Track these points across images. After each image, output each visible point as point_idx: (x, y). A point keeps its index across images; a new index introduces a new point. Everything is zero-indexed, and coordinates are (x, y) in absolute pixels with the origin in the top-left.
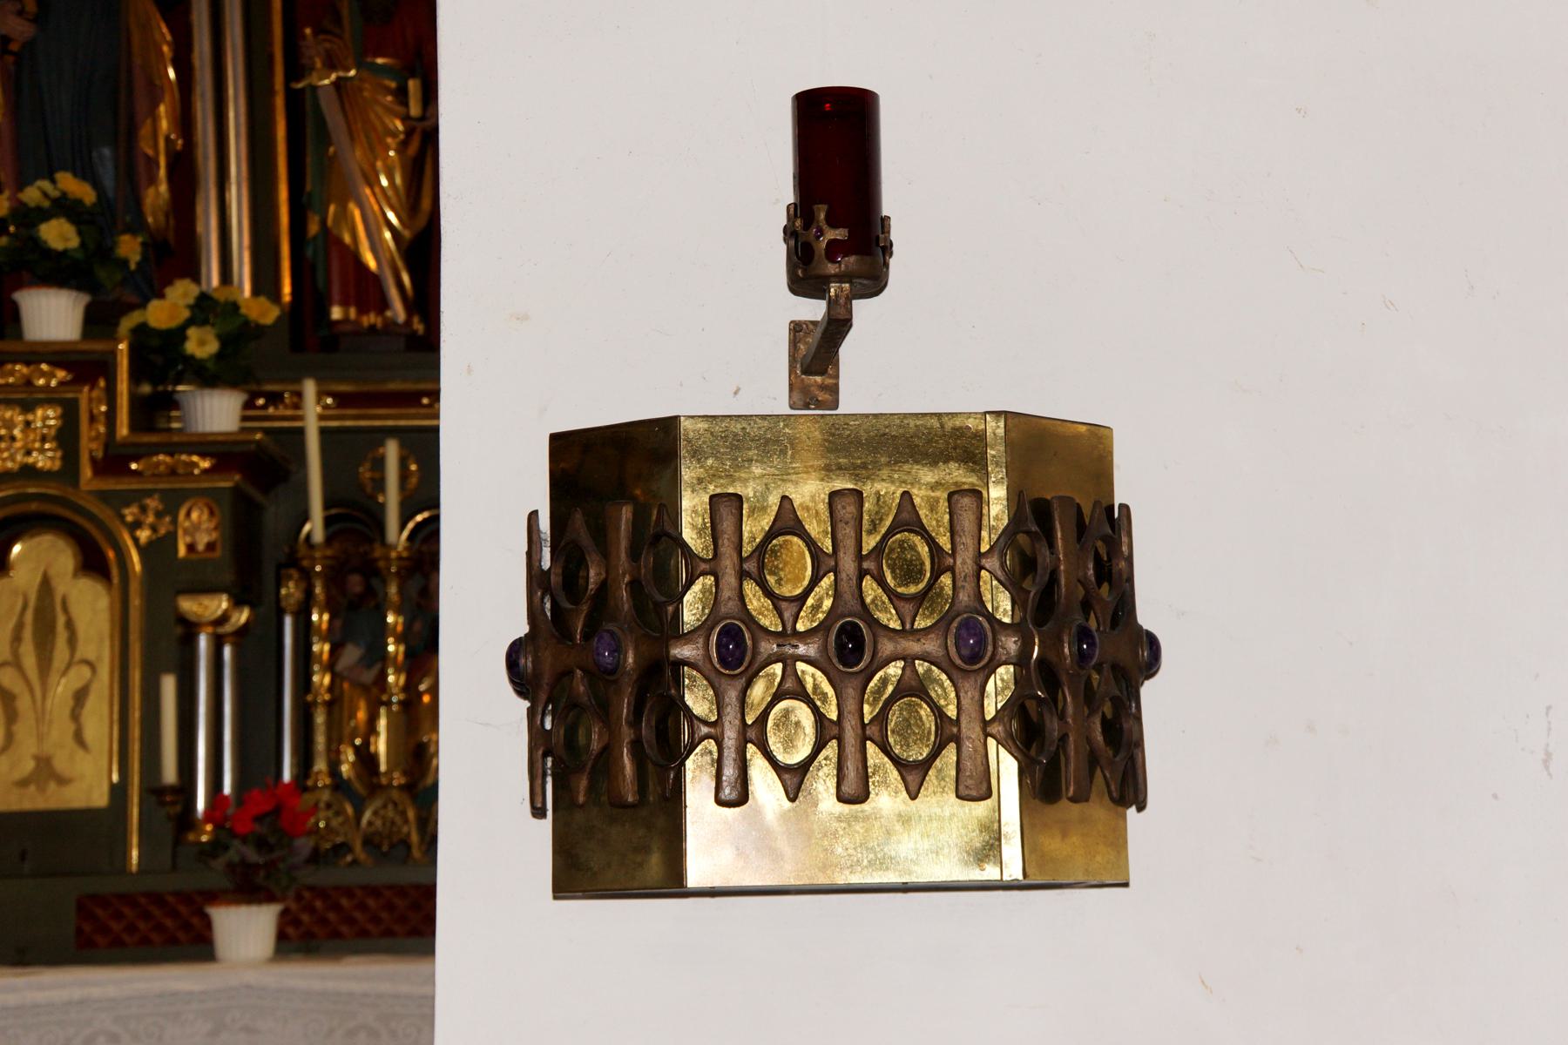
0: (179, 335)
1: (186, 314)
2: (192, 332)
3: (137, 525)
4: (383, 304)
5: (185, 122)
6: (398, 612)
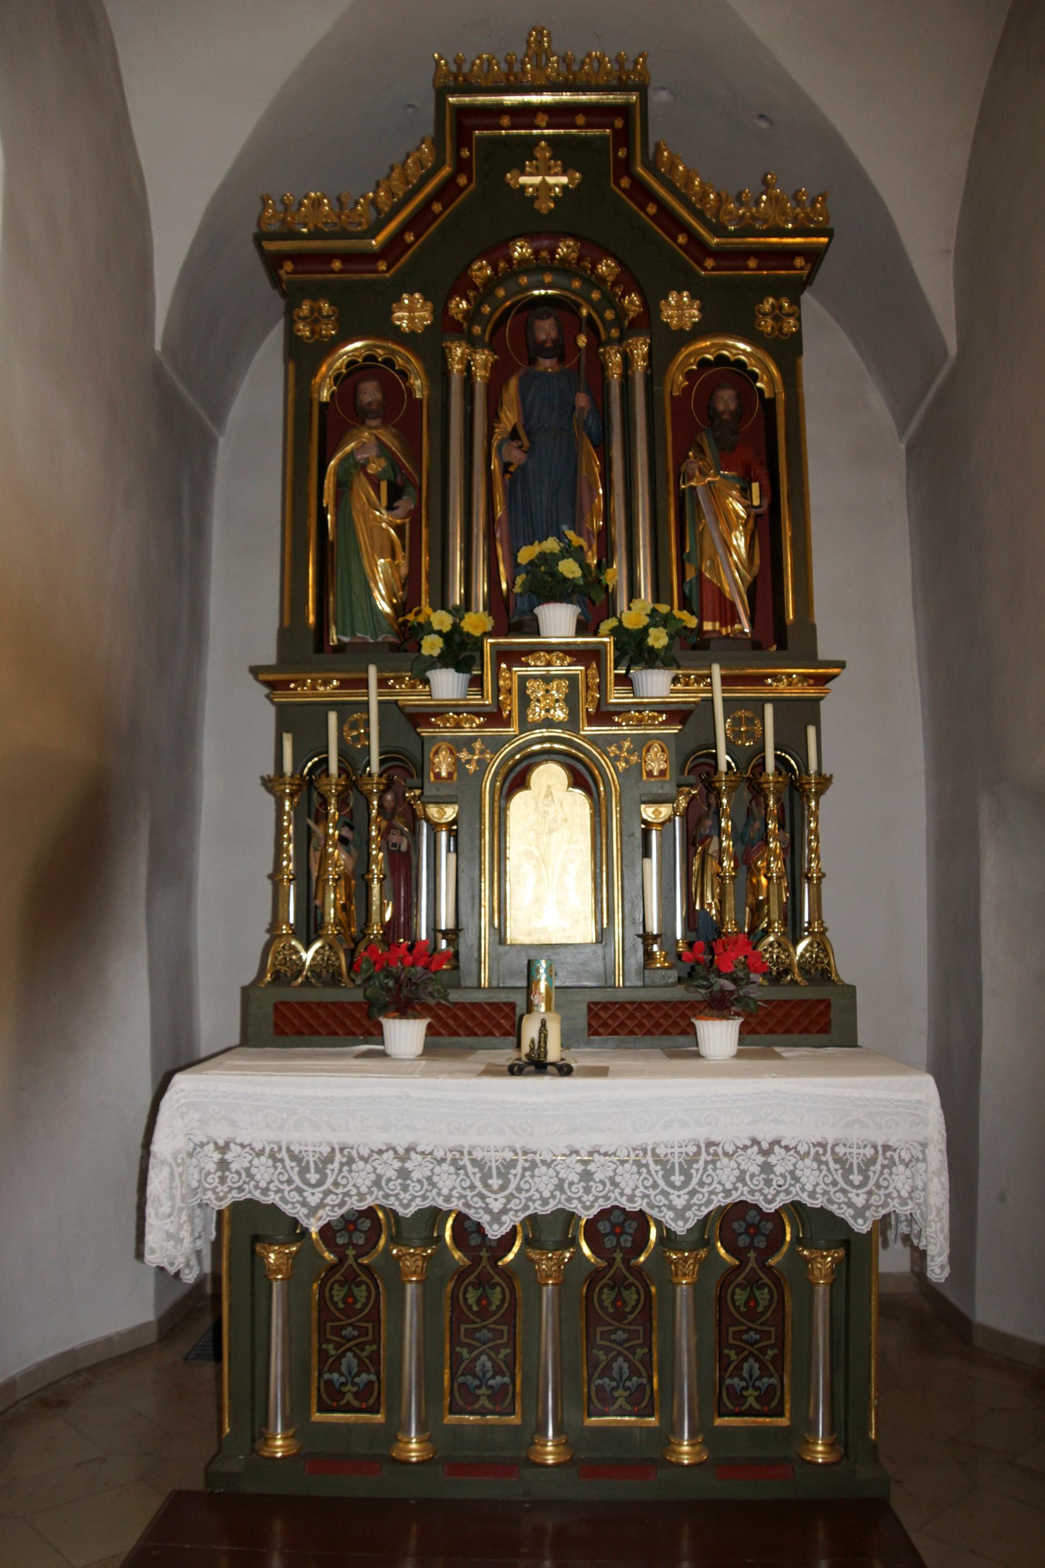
0: (644, 632)
1: (647, 620)
2: (652, 631)
3: (617, 758)
4: (735, 618)
5: (607, 516)
6: (729, 818)
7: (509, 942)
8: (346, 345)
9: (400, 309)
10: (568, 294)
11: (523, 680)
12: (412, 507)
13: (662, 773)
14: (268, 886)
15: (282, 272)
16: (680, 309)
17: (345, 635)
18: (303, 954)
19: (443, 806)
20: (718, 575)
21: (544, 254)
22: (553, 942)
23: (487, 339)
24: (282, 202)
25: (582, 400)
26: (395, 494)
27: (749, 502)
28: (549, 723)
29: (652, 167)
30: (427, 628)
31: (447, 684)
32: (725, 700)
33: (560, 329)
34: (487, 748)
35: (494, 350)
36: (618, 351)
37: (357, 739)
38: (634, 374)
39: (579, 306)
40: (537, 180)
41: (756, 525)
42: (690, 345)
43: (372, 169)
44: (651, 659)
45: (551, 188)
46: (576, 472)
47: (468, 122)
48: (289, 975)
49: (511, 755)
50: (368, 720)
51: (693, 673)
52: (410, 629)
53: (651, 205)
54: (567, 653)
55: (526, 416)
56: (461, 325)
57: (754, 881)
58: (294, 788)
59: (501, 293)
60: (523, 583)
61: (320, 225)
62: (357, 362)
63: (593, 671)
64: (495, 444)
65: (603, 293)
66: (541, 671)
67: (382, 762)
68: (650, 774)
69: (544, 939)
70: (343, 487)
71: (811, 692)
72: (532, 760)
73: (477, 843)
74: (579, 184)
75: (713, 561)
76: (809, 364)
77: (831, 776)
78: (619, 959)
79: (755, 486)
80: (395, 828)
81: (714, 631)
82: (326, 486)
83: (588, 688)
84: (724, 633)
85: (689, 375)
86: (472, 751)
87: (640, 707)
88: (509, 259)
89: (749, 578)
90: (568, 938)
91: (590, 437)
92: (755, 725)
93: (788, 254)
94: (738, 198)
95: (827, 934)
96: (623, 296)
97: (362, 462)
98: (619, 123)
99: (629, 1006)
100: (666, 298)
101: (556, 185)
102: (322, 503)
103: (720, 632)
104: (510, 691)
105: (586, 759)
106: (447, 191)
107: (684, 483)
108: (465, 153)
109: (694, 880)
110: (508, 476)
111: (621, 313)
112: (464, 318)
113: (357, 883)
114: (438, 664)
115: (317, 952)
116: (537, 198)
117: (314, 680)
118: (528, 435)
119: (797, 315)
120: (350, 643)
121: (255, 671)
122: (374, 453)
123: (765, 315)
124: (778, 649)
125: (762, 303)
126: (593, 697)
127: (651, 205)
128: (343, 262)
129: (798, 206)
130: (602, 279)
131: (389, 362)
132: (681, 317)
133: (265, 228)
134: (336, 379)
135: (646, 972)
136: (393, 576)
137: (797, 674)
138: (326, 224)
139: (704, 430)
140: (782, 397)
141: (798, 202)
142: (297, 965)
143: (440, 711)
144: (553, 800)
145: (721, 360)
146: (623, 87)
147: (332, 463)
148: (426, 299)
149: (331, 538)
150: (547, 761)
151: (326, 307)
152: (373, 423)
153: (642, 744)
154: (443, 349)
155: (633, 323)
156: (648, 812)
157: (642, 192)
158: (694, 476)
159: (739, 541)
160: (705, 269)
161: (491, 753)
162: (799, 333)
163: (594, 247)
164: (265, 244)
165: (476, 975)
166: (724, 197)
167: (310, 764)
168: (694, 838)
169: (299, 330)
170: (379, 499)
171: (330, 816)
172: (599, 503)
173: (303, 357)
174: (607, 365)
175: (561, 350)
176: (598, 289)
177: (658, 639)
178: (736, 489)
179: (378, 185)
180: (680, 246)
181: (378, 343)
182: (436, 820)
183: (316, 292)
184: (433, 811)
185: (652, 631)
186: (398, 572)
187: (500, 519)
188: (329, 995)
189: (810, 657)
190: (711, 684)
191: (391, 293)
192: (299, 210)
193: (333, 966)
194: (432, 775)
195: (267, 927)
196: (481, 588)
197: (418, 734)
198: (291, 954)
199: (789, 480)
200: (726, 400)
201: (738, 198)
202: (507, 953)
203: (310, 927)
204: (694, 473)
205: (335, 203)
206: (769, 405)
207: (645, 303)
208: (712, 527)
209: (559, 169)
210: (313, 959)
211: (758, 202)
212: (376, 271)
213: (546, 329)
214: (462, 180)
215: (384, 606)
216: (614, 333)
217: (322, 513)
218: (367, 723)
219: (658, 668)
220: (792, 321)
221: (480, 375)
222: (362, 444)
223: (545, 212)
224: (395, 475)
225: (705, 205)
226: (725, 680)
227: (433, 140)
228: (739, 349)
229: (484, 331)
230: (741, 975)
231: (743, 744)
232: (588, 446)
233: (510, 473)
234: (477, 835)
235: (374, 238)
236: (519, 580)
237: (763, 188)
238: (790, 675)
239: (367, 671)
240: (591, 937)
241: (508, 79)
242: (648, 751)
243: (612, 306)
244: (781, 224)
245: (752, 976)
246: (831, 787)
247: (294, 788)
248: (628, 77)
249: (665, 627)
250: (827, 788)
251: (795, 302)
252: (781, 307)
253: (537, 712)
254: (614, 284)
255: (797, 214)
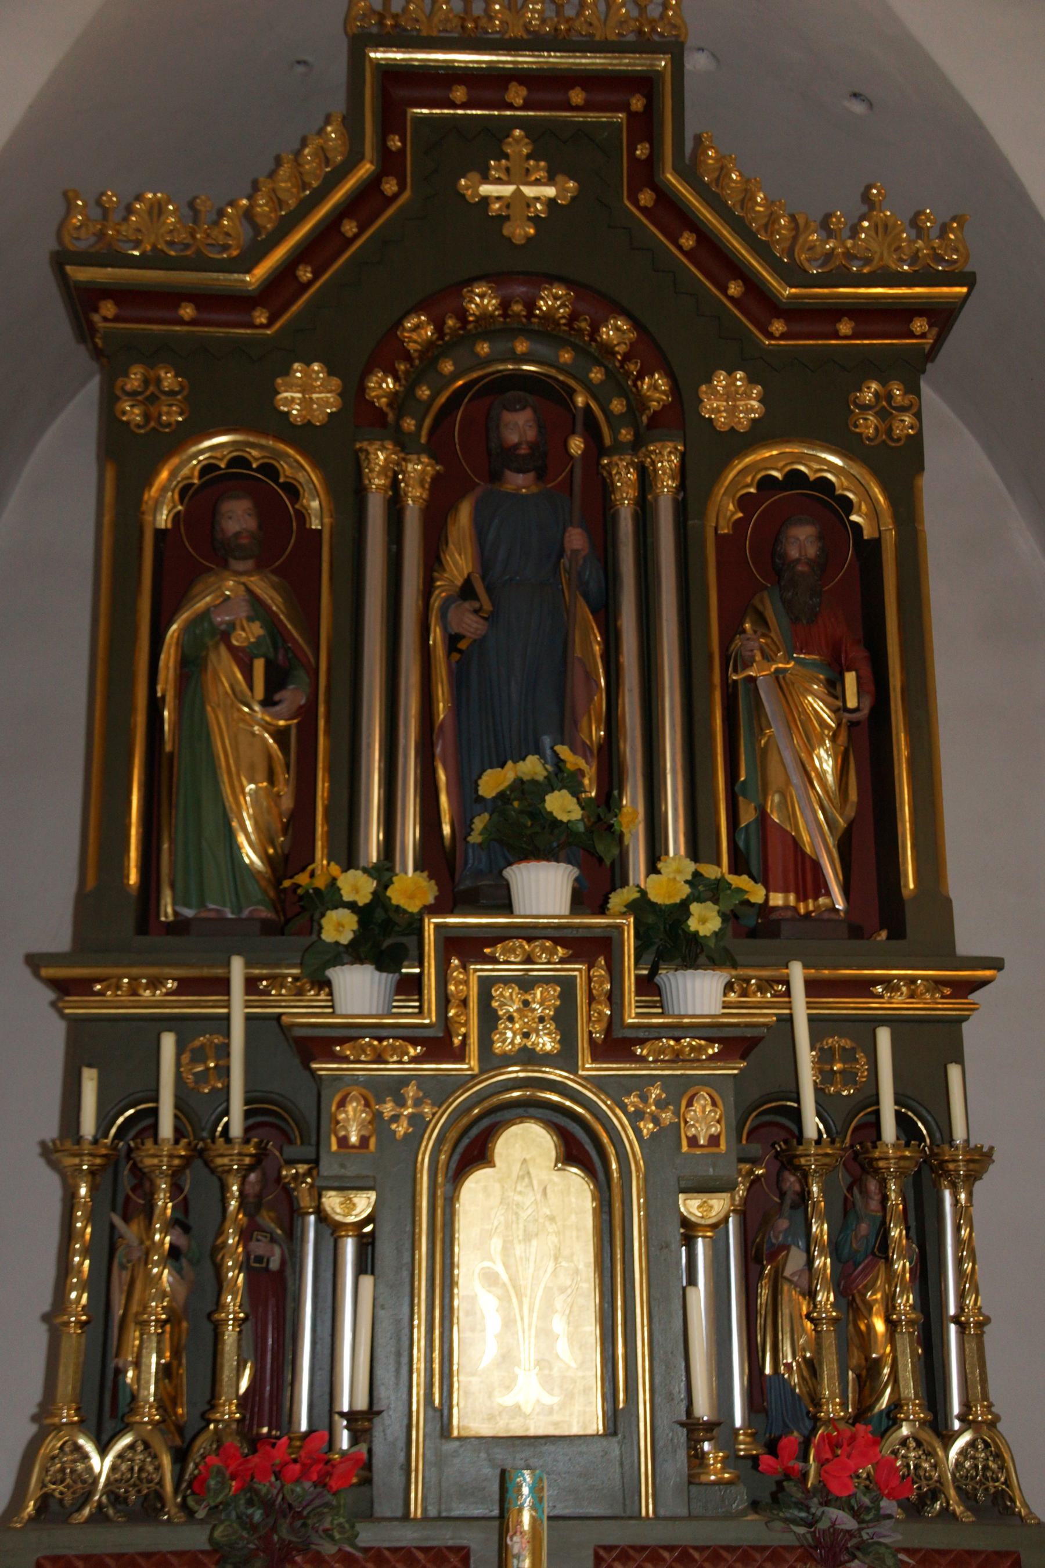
0: (683, 908)
1: (687, 890)
4: (820, 887)
5: (612, 722)
7: (455, 1433)
8: (201, 441)
9: (289, 388)
10: (553, 372)
11: (486, 985)
12: (303, 702)
13: (714, 1140)
14: (41, 1333)
15: (96, 318)
16: (731, 399)
17: (187, 905)
18: (95, 1460)
19: (352, 1194)
20: (792, 818)
21: (517, 308)
22: (532, 1432)
23: (423, 440)
24: (99, 203)
25: (576, 539)
26: (276, 681)
27: (840, 704)
28: (528, 1056)
29: (690, 173)
30: (329, 897)
31: (358, 991)
32: (811, 1019)
33: (541, 426)
34: (426, 1095)
35: (435, 457)
36: (631, 463)
37: (202, 1077)
38: (656, 498)
39: (571, 392)
40: (507, 190)
41: (850, 738)
42: (746, 455)
43: (252, 175)
44: (691, 953)
45: (529, 203)
46: (565, 652)
47: (400, 93)
48: (68, 1500)
49: (465, 1109)
50: (228, 1046)
51: (754, 975)
52: (301, 898)
53: (686, 234)
54: (557, 941)
55: (485, 562)
56: (384, 415)
57: (863, 1327)
58: (98, 1161)
59: (448, 367)
60: (485, 828)
61: (161, 246)
62: (218, 468)
63: (600, 972)
64: (436, 604)
65: (608, 372)
66: (514, 969)
67: (248, 1114)
68: (693, 1141)
69: (516, 1428)
70: (192, 666)
71: (943, 1006)
72: (497, 1117)
73: (407, 1259)
74: (573, 199)
75: (783, 795)
76: (933, 486)
77: (992, 1148)
78: (645, 1465)
79: (850, 678)
80: (261, 1229)
81: (786, 907)
82: (162, 663)
83: (591, 999)
84: (802, 911)
85: (745, 503)
86: (401, 1102)
87: (677, 1031)
88: (462, 315)
89: (842, 823)
90: (556, 1424)
91: (585, 596)
92: (857, 1061)
93: (899, 314)
94: (825, 224)
95: (999, 1426)
96: (640, 377)
97: (223, 627)
98: (637, 103)
99: (666, 1555)
100: (709, 381)
101: (537, 199)
102: (155, 692)
103: (795, 909)
104: (464, 1002)
105: (588, 1116)
106: (366, 201)
107: (736, 671)
108: (395, 143)
109: (760, 1321)
110: (456, 656)
111: (637, 403)
112: (390, 405)
113: (194, 1331)
114: (346, 958)
115: (120, 1456)
116: (507, 218)
117: (134, 979)
118: (489, 589)
119: (915, 410)
120: (195, 919)
121: (34, 962)
122: (244, 614)
123: (865, 408)
124: (889, 938)
125: (860, 391)
126: (600, 1013)
127: (686, 234)
128: (198, 308)
129: (919, 236)
130: (608, 350)
131: (269, 470)
132: (733, 411)
133: (71, 246)
134: (184, 491)
135: (694, 1489)
136: (269, 812)
137: (924, 978)
138: (171, 244)
139: (766, 588)
140: (890, 538)
141: (920, 232)
142: (84, 1482)
143: (350, 1034)
144: (531, 1184)
145: (795, 478)
146: (644, 45)
147: (174, 627)
148: (331, 372)
149: (168, 748)
150: (521, 1119)
151: (169, 379)
152: (240, 566)
153: (680, 1092)
154: (357, 452)
155: (656, 420)
156: (691, 1206)
157: (672, 213)
158: (753, 660)
159: (825, 762)
160: (770, 336)
161: (433, 1105)
162: (919, 434)
163: (596, 299)
164: (69, 269)
165: (401, 1495)
166: (801, 221)
167: (121, 1120)
168: (759, 1250)
169: (124, 413)
170: (251, 687)
171: (157, 1212)
172: (601, 701)
173: (127, 455)
174: (613, 484)
175: (543, 459)
176: (600, 364)
177: (704, 921)
178: (818, 682)
179: (255, 187)
180: (731, 299)
181: (252, 439)
182: (338, 1218)
183: (155, 353)
184: (332, 1202)
185: (694, 907)
186: (278, 805)
187: (442, 725)
188: (140, 1538)
189: (942, 951)
190: (788, 993)
191: (277, 359)
192: (126, 219)
193: (150, 1481)
194: (334, 1140)
195: (34, 1410)
196: (410, 833)
197: (313, 1072)
198: (75, 1461)
199: (904, 668)
200: (802, 541)
201: (825, 224)
202: (455, 1453)
203: (107, 1410)
204: (753, 657)
205: (186, 211)
206: (869, 551)
207: (675, 389)
208: (782, 743)
209: (542, 174)
210: (114, 1468)
211: (855, 231)
212: (252, 326)
213: (519, 426)
214: (390, 187)
215: (250, 856)
216: (626, 435)
217: (155, 707)
218: (225, 1051)
219: (704, 967)
220: (907, 420)
221: (414, 496)
222: (228, 595)
223: (519, 240)
224: (276, 648)
225: (772, 234)
226: (813, 987)
227: (344, 118)
228: (825, 462)
229: (419, 427)
230: (866, 1501)
231: (838, 1094)
232: (584, 611)
233: (460, 651)
234: (408, 1245)
235: (248, 271)
236: (479, 823)
237: (864, 209)
238: (912, 981)
239: (228, 965)
240: (596, 1426)
241: (463, 27)
242: (690, 1104)
243: (623, 392)
244: (893, 266)
245: (884, 1503)
246: (992, 1168)
247: (98, 1161)
248: (653, 30)
249: (716, 902)
250: (985, 1169)
251: (913, 388)
252: (890, 397)
253: (508, 1039)
254: (627, 357)
255: (918, 250)
